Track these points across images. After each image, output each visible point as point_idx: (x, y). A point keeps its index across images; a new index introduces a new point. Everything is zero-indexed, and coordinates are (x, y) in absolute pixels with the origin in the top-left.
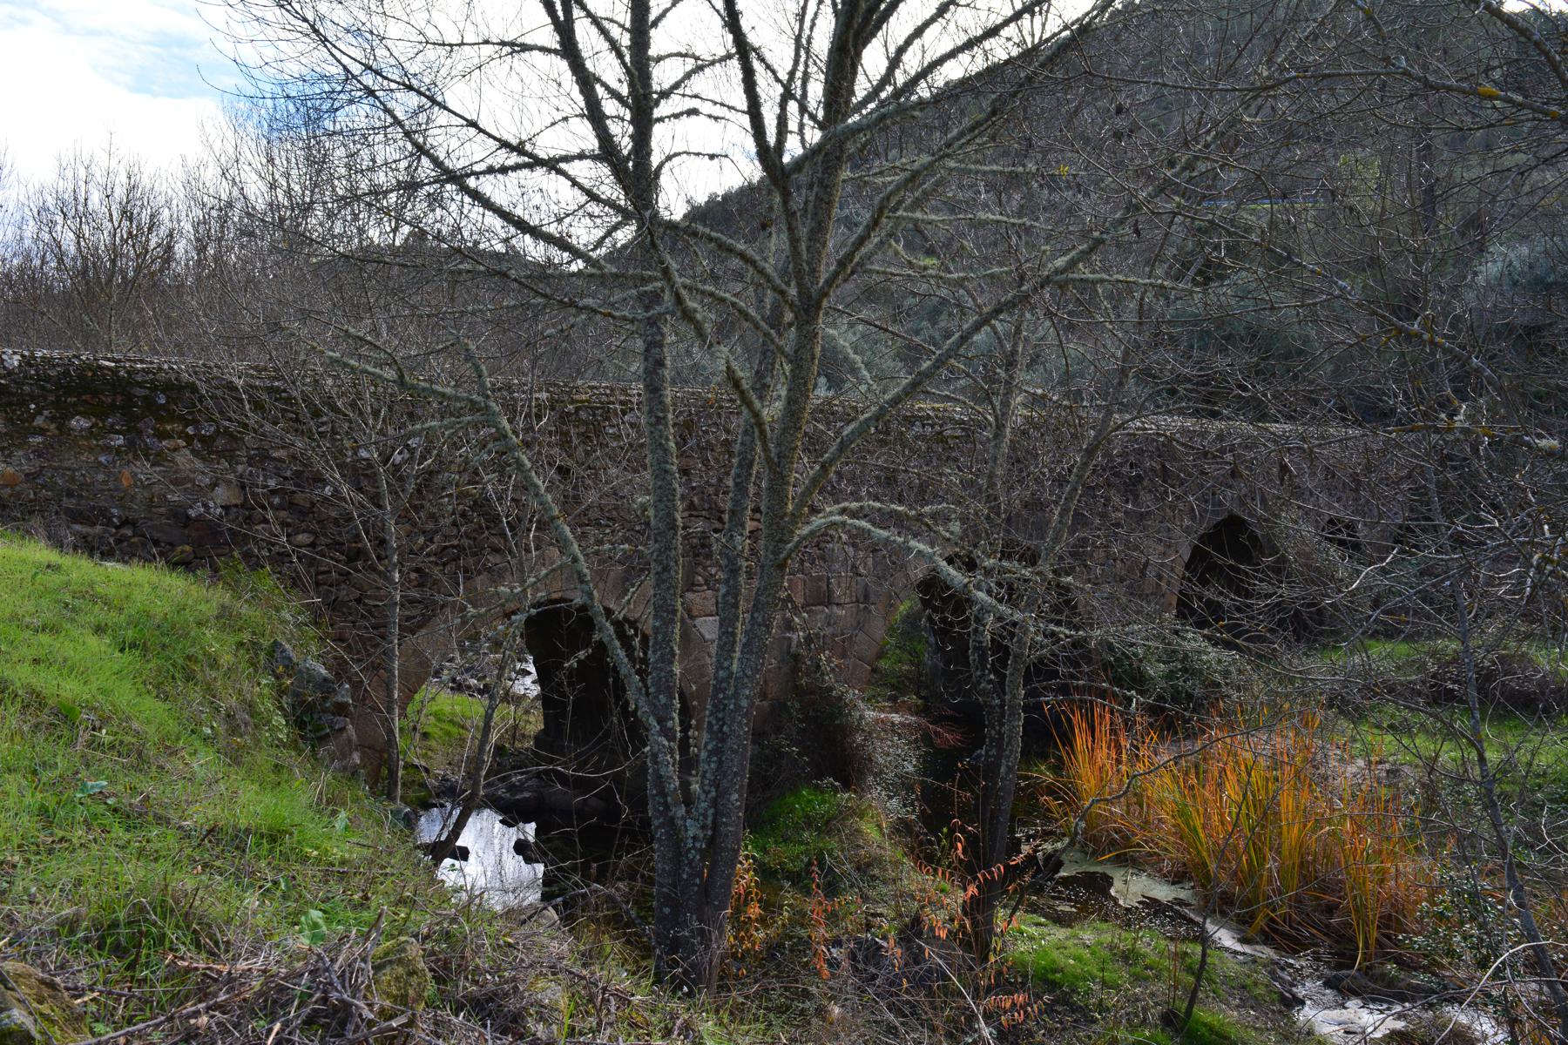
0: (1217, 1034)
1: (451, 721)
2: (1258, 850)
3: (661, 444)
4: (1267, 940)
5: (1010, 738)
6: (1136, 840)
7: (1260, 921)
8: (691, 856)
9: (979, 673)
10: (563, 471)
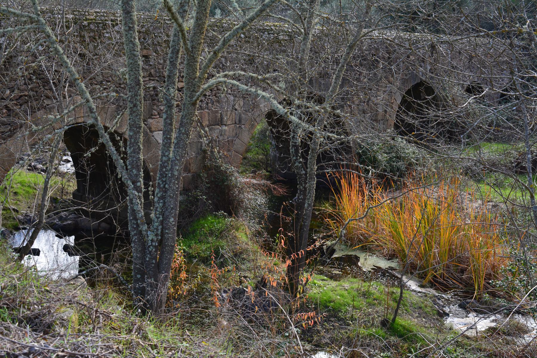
0: (407, 330)
1: (29, 186)
2: (429, 243)
3: (131, 41)
4: (432, 285)
5: (310, 190)
6: (371, 239)
7: (429, 277)
8: (150, 250)
9: (295, 158)
10: (82, 56)
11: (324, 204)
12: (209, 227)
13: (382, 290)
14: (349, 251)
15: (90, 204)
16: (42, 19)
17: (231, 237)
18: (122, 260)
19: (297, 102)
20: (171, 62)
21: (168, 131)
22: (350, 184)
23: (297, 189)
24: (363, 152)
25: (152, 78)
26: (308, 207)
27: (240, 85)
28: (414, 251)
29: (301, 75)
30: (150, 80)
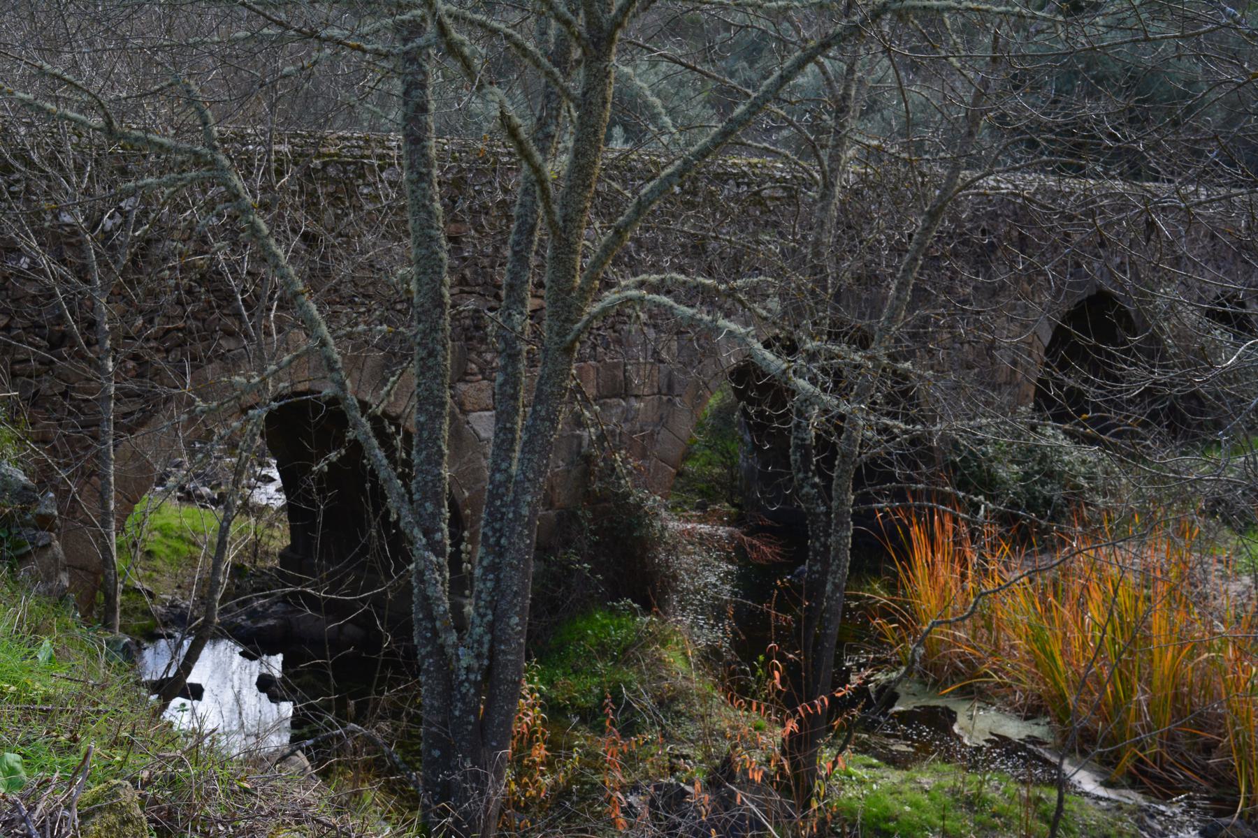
1: (180, 538)
2: (1125, 681)
3: (424, 206)
4: (1135, 784)
5: (837, 551)
6: (984, 669)
7: (1127, 762)
9: (801, 475)
10: (309, 239)
11: (868, 584)
12: (596, 635)
13: (1012, 791)
14: (932, 698)
15: (322, 581)
16: (221, 157)
17: (648, 661)
18: (396, 715)
19: (810, 345)
20: (515, 253)
21: (508, 414)
22: (932, 539)
23: (808, 549)
24: (964, 460)
25: (466, 289)
26: (833, 592)
27: (676, 305)
28: (1088, 698)
29: (814, 281)
30: (462, 292)
